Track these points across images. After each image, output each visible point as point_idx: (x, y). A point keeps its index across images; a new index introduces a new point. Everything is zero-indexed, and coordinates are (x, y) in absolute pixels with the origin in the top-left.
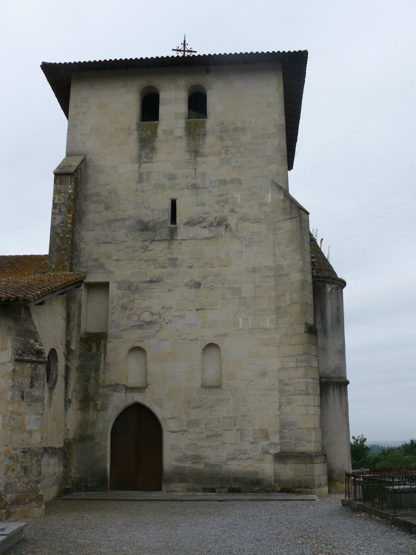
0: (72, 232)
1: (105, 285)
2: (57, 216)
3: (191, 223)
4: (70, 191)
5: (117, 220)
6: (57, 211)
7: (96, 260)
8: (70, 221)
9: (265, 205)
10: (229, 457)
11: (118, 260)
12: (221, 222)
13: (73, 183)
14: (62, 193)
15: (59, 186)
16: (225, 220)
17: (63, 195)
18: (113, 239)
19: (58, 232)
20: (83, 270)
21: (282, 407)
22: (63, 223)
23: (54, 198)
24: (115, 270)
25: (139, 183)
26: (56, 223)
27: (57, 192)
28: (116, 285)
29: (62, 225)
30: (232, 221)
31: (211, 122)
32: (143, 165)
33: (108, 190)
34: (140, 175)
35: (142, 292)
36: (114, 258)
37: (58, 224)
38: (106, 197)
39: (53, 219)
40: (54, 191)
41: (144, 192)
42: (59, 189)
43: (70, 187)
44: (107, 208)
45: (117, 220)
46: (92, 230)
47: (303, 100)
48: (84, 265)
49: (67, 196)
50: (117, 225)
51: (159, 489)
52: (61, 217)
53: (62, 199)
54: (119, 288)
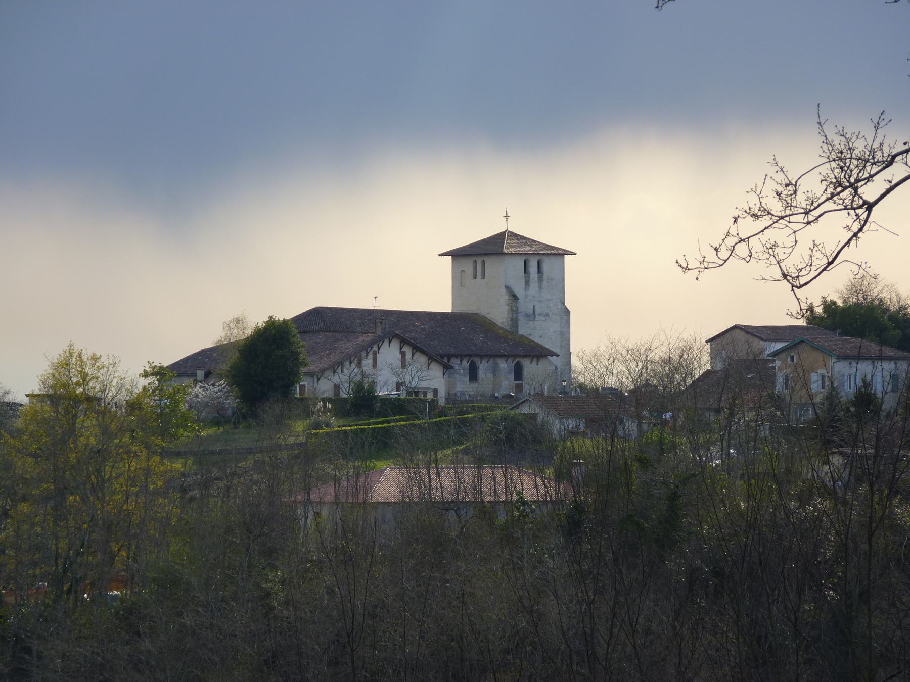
3: (539, 315)
9: (558, 309)
10: (344, 424)
12: (547, 315)
16: (548, 314)
20: (843, 373)
21: (233, 426)
30: (550, 315)
31: (545, 277)
47: (464, 245)
51: (516, 384)
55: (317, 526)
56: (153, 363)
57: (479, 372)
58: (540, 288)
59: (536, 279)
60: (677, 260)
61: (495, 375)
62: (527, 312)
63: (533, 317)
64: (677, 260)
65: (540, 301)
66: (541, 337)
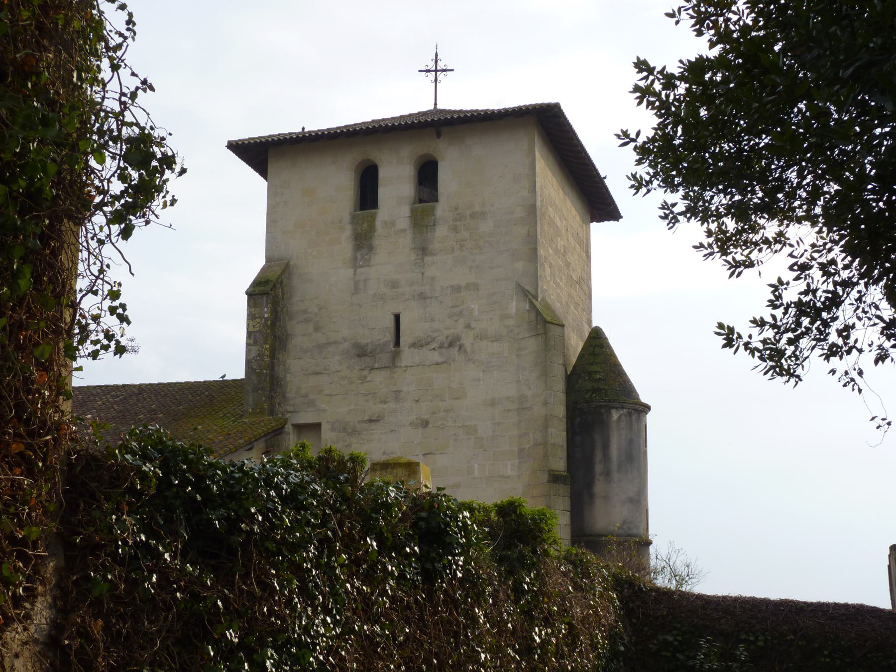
0: (272, 366)
1: (317, 427)
2: (252, 348)
3: (417, 345)
4: (266, 315)
5: (329, 344)
6: (252, 341)
7: (306, 396)
8: (267, 353)
9: (508, 317)
11: (331, 395)
12: (453, 342)
13: (270, 305)
14: (256, 318)
15: (253, 309)
16: (458, 338)
17: (258, 320)
18: (325, 369)
19: (255, 367)
22: (259, 356)
23: (248, 325)
24: (327, 408)
25: (353, 294)
26: (252, 356)
27: (251, 317)
28: (329, 427)
29: (258, 358)
30: (467, 341)
31: (442, 208)
32: (359, 270)
33: (318, 305)
34: (356, 283)
35: (359, 434)
36: (326, 392)
37: (254, 357)
38: (316, 315)
39: (248, 352)
40: (248, 315)
41: (360, 306)
42: (253, 313)
43: (266, 309)
44: (317, 329)
45: (329, 344)
46: (300, 358)
48: (292, 402)
49: (263, 321)
50: (329, 350)
52: (257, 348)
53: (257, 326)
54: (333, 430)
55: (422, 346)
56: (638, 134)
57: (577, 210)
58: (423, 250)
59: (404, 222)
60: (152, 89)
61: (367, 420)
62: (364, 341)
63: (385, 359)
64: (152, 89)
65: (422, 297)
66: (425, 424)
